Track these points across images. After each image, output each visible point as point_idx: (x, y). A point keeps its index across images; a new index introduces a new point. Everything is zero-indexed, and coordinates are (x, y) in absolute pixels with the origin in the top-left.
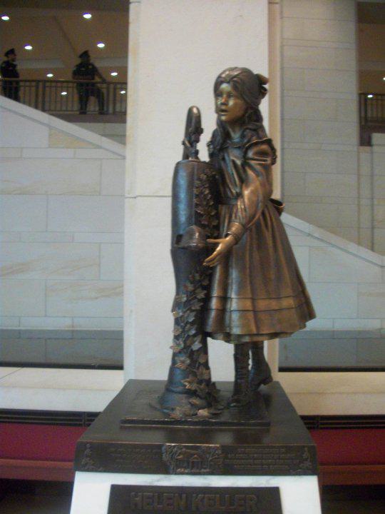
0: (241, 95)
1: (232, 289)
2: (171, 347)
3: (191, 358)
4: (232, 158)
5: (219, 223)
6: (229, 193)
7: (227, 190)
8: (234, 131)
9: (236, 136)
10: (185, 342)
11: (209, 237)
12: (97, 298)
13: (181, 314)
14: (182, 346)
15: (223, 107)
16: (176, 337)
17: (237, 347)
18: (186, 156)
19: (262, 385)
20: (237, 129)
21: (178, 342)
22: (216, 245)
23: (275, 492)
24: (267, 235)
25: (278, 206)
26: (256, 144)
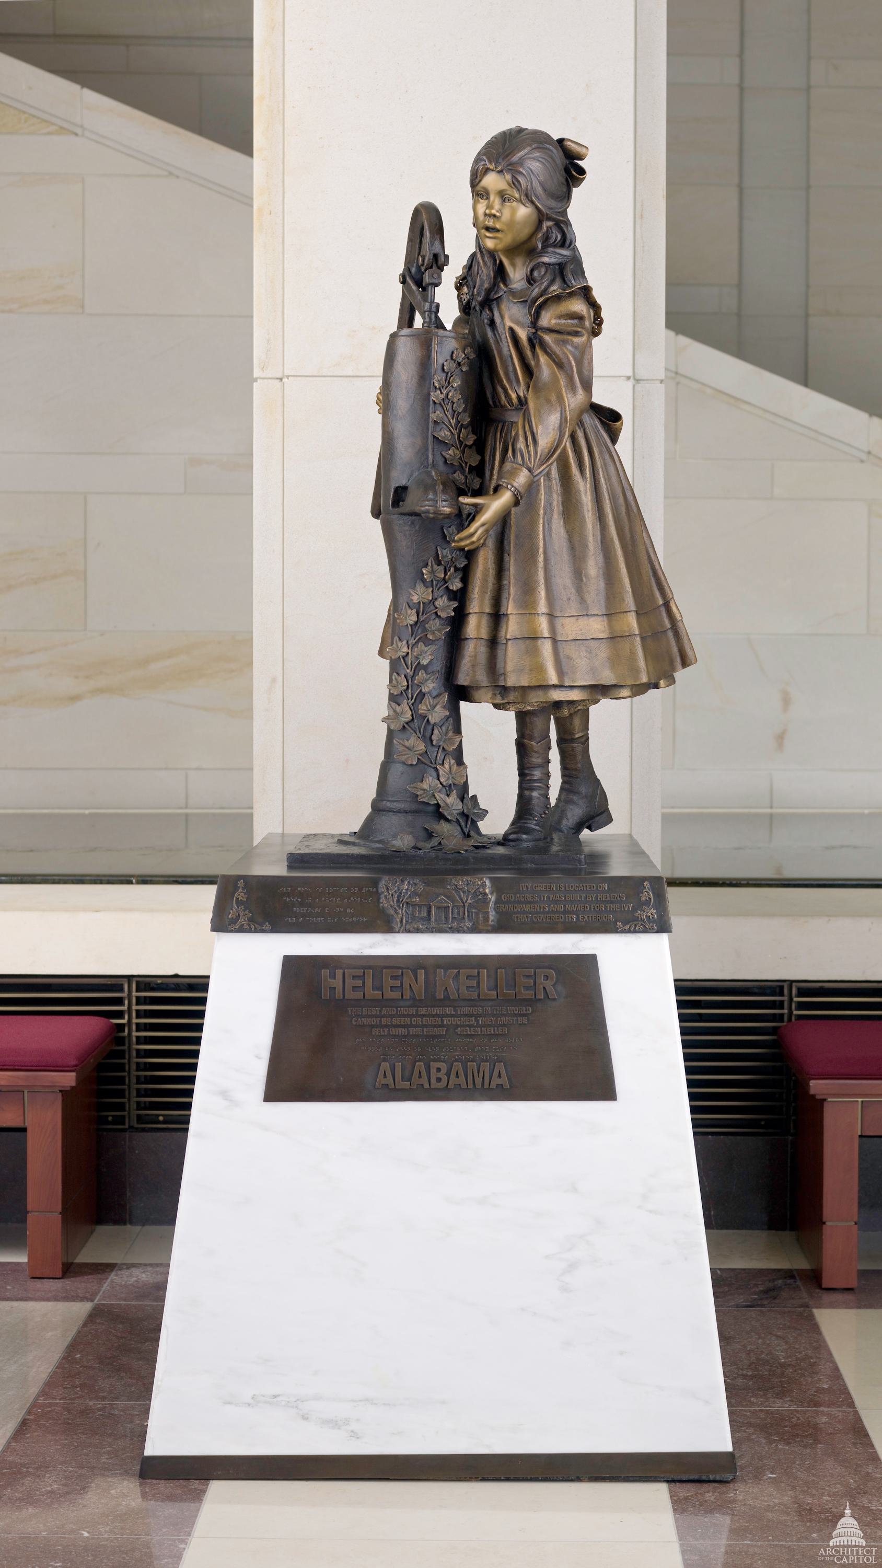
0: (527, 195)
1: (509, 595)
2: (384, 720)
3: (421, 738)
4: (508, 323)
5: (482, 484)
6: (503, 400)
7: (500, 390)
8: (513, 265)
9: (517, 274)
10: (413, 708)
11: (462, 492)
12: (75, 698)
13: (405, 650)
14: (408, 715)
15: (490, 223)
16: (394, 699)
17: (522, 718)
18: (406, 319)
19: (586, 832)
20: (519, 261)
21: (398, 709)
22: (478, 510)
23: (588, 963)
24: (582, 489)
25: (610, 419)
26: (558, 298)
